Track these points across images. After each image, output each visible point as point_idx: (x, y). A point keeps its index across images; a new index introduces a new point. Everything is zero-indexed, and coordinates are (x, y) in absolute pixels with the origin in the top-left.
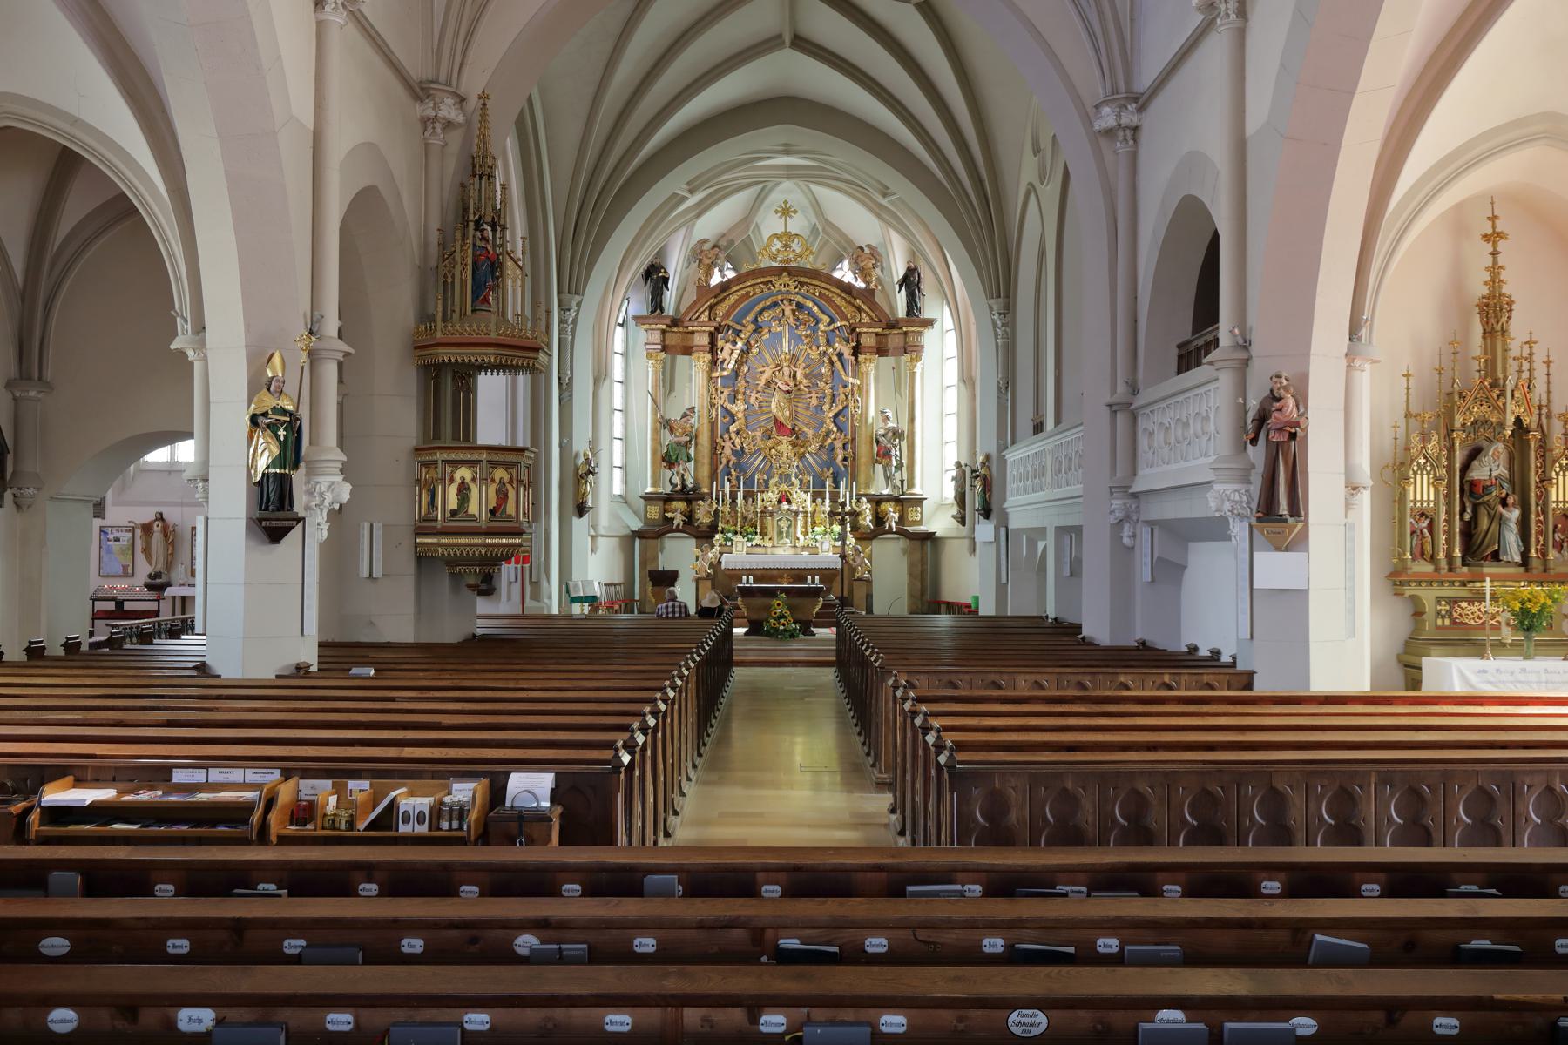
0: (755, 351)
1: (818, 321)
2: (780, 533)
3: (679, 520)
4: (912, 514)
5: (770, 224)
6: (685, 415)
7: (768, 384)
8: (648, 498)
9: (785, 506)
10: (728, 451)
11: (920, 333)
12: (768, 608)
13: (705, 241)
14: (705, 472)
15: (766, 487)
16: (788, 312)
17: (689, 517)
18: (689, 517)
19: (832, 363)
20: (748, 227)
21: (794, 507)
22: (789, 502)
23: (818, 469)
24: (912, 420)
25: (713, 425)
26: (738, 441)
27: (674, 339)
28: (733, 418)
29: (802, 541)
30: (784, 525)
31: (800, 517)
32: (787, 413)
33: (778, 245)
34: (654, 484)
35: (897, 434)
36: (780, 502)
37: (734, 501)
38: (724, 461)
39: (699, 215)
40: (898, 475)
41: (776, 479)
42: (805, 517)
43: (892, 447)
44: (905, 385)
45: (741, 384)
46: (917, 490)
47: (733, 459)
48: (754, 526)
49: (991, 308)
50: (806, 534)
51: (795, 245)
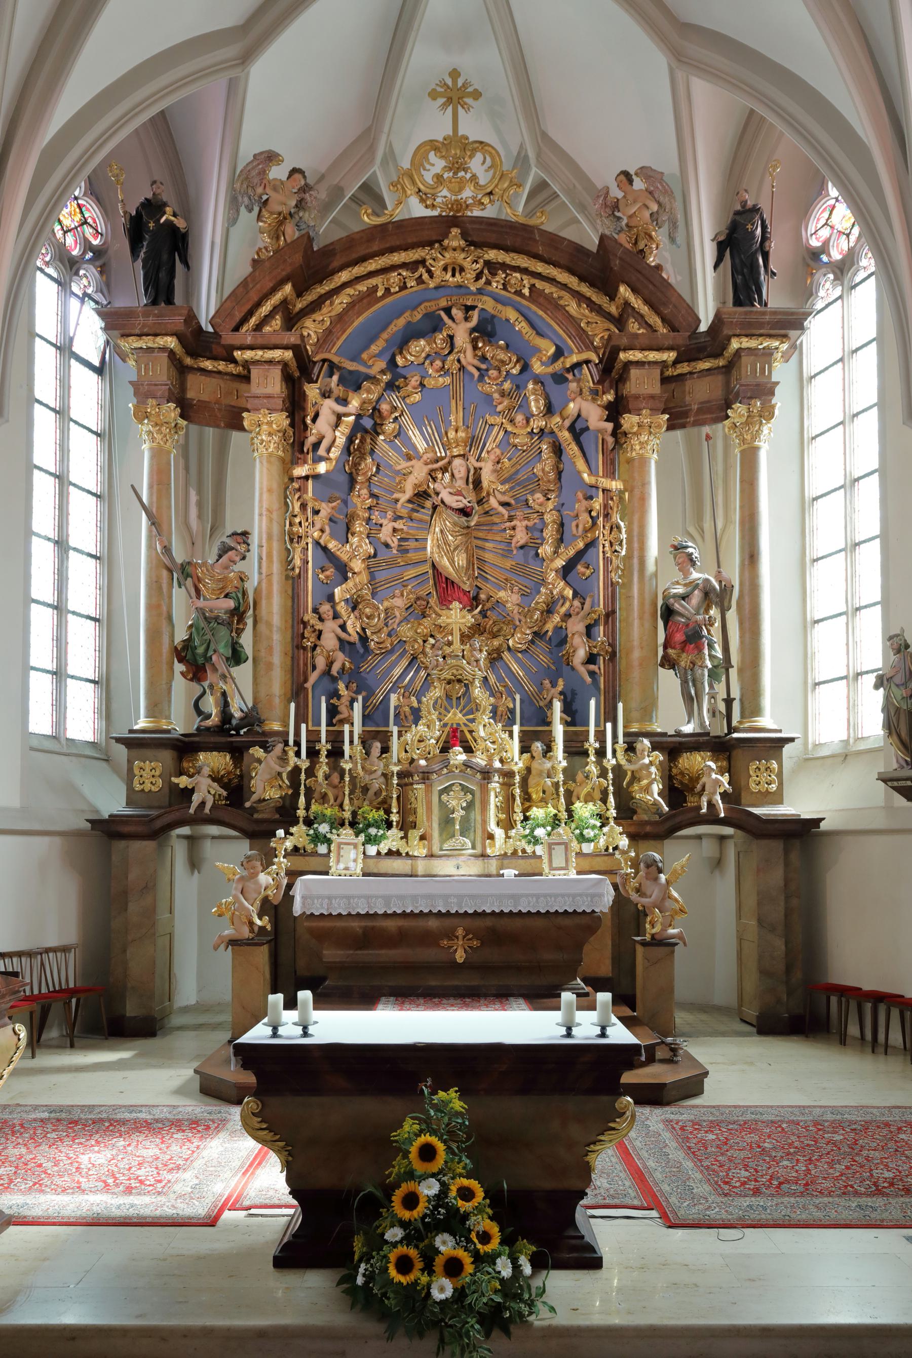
0: (389, 427)
2: (447, 822)
3: (205, 792)
4: (758, 777)
7: (421, 495)
8: (136, 743)
9: (458, 756)
10: (329, 641)
11: (768, 354)
12: (383, 1147)
13: (271, 157)
14: (277, 683)
16: (462, 338)
17: (235, 790)
18: (235, 790)
19: (558, 450)
20: (372, 149)
21: (480, 760)
22: (468, 750)
24: (751, 557)
25: (294, 582)
26: (353, 625)
27: (189, 372)
28: (343, 571)
29: (500, 843)
31: (495, 785)
32: (461, 559)
33: (437, 164)
34: (156, 707)
35: (717, 596)
37: (336, 753)
38: (321, 662)
39: (246, 57)
40: (720, 688)
41: (437, 692)
42: (507, 786)
43: (701, 629)
45: (360, 499)
46: (769, 721)
47: (341, 659)
48: (389, 808)
50: (508, 825)
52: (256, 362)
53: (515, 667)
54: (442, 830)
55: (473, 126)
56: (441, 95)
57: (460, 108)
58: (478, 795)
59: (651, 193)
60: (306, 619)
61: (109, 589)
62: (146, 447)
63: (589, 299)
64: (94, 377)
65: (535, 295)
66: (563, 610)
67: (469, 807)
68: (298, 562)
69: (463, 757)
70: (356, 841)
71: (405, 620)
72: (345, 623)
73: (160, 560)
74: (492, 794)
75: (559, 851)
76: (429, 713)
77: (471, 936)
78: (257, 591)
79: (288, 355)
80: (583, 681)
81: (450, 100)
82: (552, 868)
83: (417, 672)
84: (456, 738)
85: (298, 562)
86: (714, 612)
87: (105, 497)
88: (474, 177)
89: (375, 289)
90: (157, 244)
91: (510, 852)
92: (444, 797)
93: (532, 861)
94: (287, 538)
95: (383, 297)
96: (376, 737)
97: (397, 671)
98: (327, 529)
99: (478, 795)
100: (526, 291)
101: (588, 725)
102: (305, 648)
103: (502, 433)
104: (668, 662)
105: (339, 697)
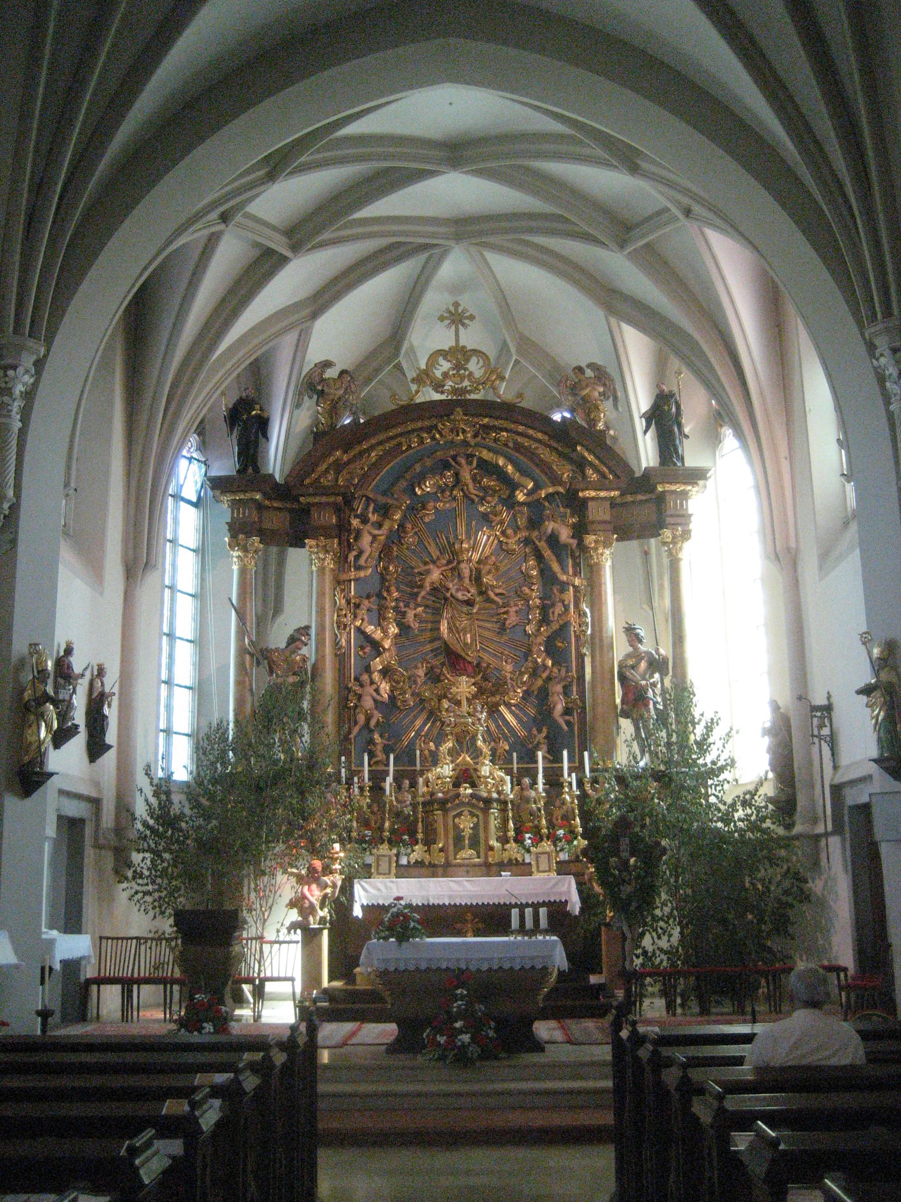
1: (514, 487)
2: (458, 840)
5: (428, 338)
6: (292, 640)
10: (368, 703)
11: (685, 495)
13: (327, 364)
15: (434, 759)
20: (398, 348)
22: (473, 785)
23: (522, 733)
24: (678, 639)
25: (341, 658)
28: (376, 647)
30: (466, 824)
31: (494, 812)
35: (657, 665)
36: (457, 784)
38: (361, 718)
39: (315, 315)
42: (504, 811)
44: (662, 586)
47: (377, 716)
49: (871, 347)
50: (504, 840)
51: (474, 366)
52: (314, 504)
53: (509, 717)
54: (455, 845)
55: (470, 338)
56: (446, 318)
57: (460, 327)
58: (481, 817)
59: (599, 378)
60: (350, 685)
61: (201, 664)
62: (235, 568)
63: (557, 449)
64: (193, 510)
65: (518, 447)
66: (544, 675)
67: (475, 827)
68: (343, 642)
69: (469, 791)
70: (390, 853)
71: (425, 683)
72: (379, 687)
73: (246, 649)
74: (492, 817)
75: (543, 859)
76: (445, 758)
77: (477, 920)
78: (315, 667)
79: (340, 499)
80: (561, 728)
81: (453, 322)
82: (539, 871)
83: (434, 722)
84: (466, 776)
85: (343, 642)
86: (657, 676)
87: (199, 596)
88: (471, 374)
89: (400, 444)
90: (247, 422)
91: (506, 861)
92: (457, 820)
93: (522, 867)
94: (335, 625)
95: (407, 450)
96: (408, 777)
97: (418, 723)
98: (365, 617)
99: (481, 817)
100: (511, 444)
101: (562, 762)
102: (349, 708)
103: (496, 542)
104: (626, 714)
105: (375, 744)
